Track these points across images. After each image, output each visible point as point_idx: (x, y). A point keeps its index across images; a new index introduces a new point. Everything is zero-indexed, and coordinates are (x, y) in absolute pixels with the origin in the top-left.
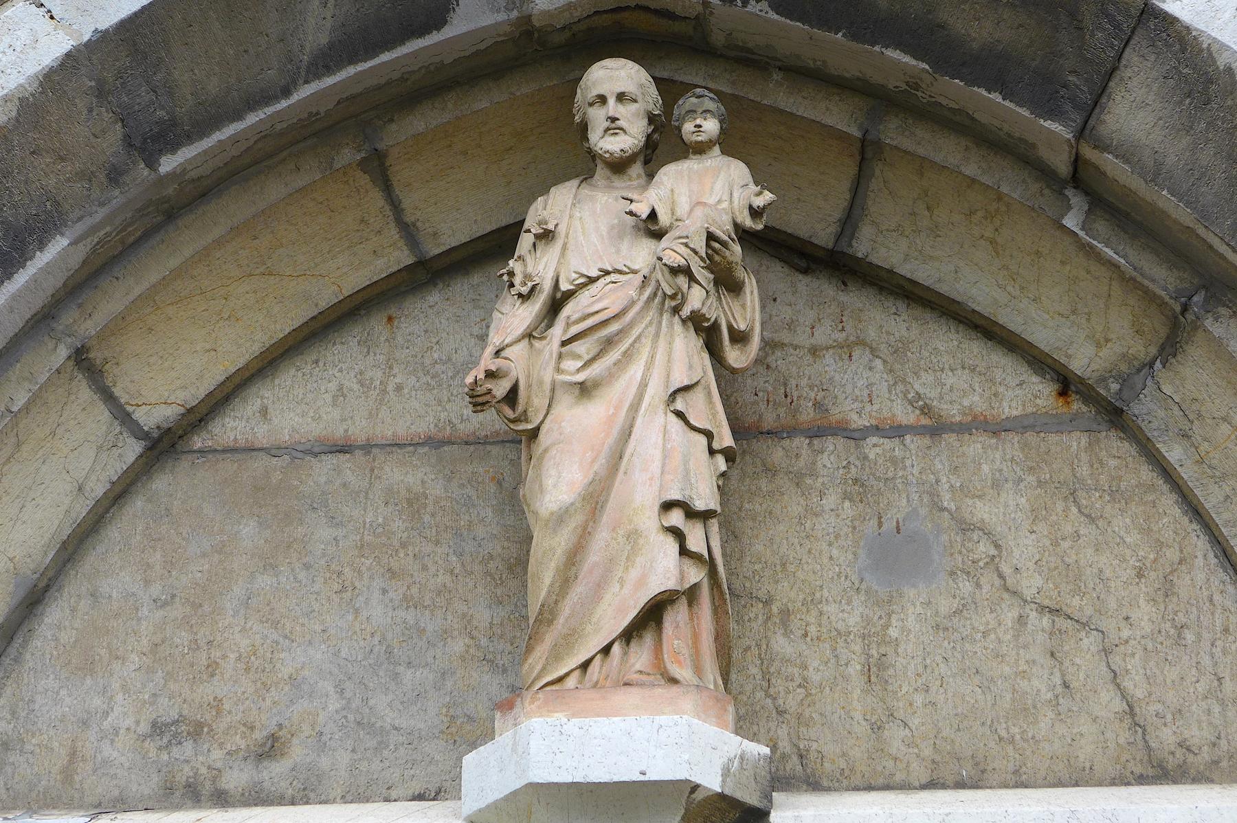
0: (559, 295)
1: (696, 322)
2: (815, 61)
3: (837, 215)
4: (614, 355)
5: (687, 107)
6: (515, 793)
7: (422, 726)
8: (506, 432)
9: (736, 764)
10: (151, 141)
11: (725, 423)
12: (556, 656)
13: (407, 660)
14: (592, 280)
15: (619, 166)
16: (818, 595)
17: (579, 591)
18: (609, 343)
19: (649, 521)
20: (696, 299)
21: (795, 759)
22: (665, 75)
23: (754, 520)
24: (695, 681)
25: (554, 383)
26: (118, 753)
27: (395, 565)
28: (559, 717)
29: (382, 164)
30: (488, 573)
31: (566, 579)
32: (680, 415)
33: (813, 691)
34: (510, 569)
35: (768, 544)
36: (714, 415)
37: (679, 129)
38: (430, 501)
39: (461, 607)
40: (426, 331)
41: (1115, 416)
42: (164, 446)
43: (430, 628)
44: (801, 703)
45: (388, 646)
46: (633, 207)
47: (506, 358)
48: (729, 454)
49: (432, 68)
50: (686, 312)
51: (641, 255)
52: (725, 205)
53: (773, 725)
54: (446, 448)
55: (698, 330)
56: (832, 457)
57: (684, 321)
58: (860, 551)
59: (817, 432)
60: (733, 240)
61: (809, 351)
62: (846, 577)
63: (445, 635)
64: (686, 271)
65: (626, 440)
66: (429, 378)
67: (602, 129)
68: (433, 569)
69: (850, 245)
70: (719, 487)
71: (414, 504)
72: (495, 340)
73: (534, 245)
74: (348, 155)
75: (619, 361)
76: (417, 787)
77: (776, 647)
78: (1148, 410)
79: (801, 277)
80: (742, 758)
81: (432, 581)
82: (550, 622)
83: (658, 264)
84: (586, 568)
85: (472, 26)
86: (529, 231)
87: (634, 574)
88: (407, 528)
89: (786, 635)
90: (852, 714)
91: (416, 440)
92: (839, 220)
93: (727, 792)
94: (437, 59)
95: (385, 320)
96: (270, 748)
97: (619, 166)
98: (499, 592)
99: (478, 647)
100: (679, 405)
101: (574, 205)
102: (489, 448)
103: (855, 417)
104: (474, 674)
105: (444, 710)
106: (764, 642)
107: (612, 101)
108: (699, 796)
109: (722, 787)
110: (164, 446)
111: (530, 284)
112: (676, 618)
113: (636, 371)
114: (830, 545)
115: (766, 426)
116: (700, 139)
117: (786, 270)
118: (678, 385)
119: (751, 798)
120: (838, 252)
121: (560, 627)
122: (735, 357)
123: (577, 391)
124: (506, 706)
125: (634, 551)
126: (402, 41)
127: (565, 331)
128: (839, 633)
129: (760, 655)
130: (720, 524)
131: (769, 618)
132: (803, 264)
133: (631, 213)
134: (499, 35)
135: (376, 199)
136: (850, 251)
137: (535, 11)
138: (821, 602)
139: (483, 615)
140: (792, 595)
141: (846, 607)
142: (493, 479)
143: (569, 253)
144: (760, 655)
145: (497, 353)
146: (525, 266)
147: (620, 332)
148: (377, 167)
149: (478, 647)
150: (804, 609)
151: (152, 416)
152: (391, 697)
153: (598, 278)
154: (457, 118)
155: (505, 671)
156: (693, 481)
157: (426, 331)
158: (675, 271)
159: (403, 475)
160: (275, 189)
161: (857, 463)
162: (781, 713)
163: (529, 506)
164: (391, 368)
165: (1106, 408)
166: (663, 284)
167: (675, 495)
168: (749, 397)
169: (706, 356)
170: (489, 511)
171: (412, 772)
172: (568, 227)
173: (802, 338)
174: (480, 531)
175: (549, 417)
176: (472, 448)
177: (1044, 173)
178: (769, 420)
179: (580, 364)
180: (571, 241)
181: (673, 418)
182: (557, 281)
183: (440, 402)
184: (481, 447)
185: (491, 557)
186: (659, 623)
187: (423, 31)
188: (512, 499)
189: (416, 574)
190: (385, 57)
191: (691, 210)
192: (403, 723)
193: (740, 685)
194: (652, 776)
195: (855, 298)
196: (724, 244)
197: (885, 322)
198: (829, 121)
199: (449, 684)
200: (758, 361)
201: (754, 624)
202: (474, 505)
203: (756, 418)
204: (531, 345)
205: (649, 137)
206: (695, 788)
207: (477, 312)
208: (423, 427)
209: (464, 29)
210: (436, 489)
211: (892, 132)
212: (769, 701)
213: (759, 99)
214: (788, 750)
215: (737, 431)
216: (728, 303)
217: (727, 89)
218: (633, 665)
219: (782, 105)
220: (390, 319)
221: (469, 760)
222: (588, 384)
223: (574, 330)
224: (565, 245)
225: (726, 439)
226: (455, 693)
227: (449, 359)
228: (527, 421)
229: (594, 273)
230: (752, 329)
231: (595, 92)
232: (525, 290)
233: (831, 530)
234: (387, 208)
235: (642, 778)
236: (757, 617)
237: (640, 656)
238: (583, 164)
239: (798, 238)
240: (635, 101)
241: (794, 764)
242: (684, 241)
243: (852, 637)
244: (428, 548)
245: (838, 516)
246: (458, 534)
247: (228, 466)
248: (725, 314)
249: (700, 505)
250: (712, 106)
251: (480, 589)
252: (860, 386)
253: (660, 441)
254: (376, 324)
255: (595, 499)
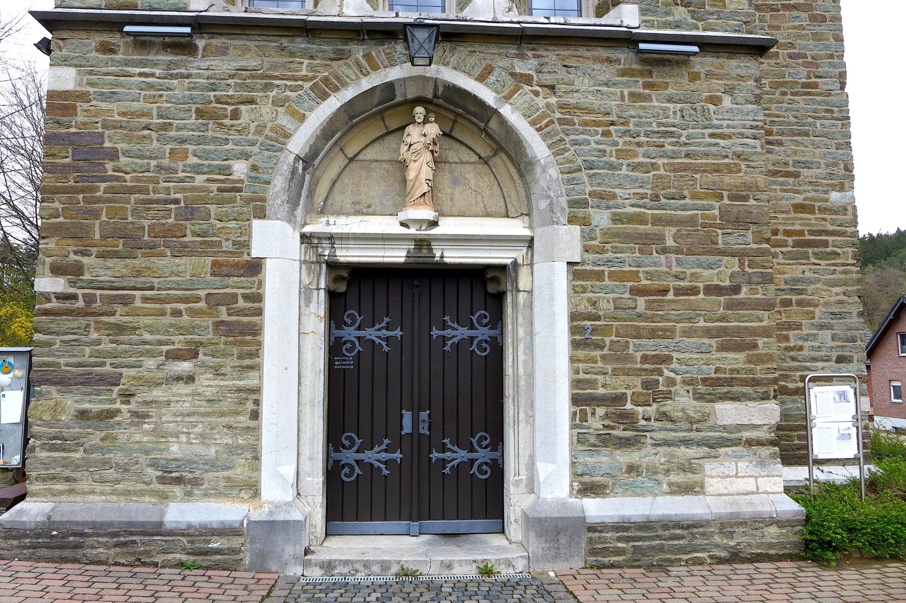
10: (351, 118)
19: (424, 181)
26: (348, 206)
41: (486, 163)
42: (351, 160)
51: (423, 139)
59: (445, 163)
65: (420, 169)
71: (388, 170)
74: (379, 118)
78: (490, 163)
96: (369, 206)
110: (351, 160)
130: (544, 461)
135: (382, 123)
139: (398, 188)
148: (383, 119)
151: (349, 156)
159: (385, 166)
160: (368, 123)
165: (485, 161)
177: (480, 128)
195: (451, 141)
197: (456, 145)
208: (389, 158)
211: (459, 120)
237: (422, 199)
247: (360, 163)
252: (452, 156)
254: (381, 141)
255: (416, 177)
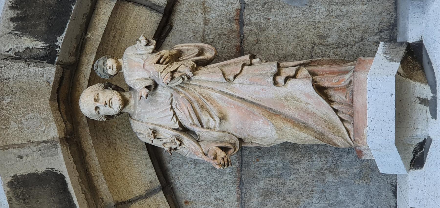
0: (181, 129)
1: (194, 70)
2: (83, 19)
3: (149, 12)
4: (208, 105)
5: (101, 72)
6: (399, 150)
7: (363, 192)
8: (237, 154)
9: (388, 56)
11: (239, 59)
12: (339, 132)
13: (335, 197)
14: (175, 114)
15: (125, 102)
16: (312, 23)
17: (310, 122)
18: (202, 107)
20: (184, 68)
21: (382, 34)
22: (87, 82)
23: (279, 49)
24: (351, 73)
25: (219, 131)
27: (294, 202)
28: (366, 131)
29: (121, 203)
30: (298, 162)
31: (306, 127)
32: (235, 77)
33: (353, 26)
34: (297, 153)
35: (289, 43)
36: (235, 63)
37: (111, 76)
38: (266, 187)
39: (313, 174)
40: (192, 187)
43: (321, 188)
44: (358, 31)
45: (329, 205)
46: (144, 96)
47: (208, 151)
48: (253, 57)
49: (80, 181)
50: (190, 74)
51: (163, 93)
52: (144, 57)
53: (367, 43)
54: (243, 180)
55: (197, 69)
56: (252, 16)
57: (194, 75)
58: (293, 5)
60: (160, 53)
61: (206, 25)
62: (304, 11)
63: (324, 181)
64: (173, 72)
66: (212, 187)
67: (110, 109)
68: (296, 186)
69: (162, 7)
70: (266, 62)
71: (267, 194)
72: (200, 157)
73: (158, 139)
75: (211, 103)
76: (390, 195)
77: (334, 41)
79: (174, 28)
80: (385, 54)
81: (301, 186)
82: (323, 135)
83: (169, 85)
84: (300, 119)
85: (63, 163)
86: (152, 141)
87: (304, 98)
88: (278, 197)
89: (328, 37)
90: (363, 10)
91: (239, 192)
92: (151, 11)
93: (400, 60)
94: (77, 178)
95: (187, 205)
97: (125, 102)
98: (306, 158)
99: (330, 167)
100: (231, 77)
101: (141, 121)
102: (244, 162)
103: (235, 6)
104: (342, 169)
105: (357, 182)
106: (331, 46)
107: (98, 104)
108: (402, 72)
109: (398, 62)
111: (176, 141)
112: (323, 82)
113: (215, 95)
114: (290, 17)
115: (238, 43)
116: (115, 67)
117: (171, 34)
118: (223, 78)
119: (402, 51)
120: (164, 12)
121: (325, 131)
122: (208, 55)
123: (224, 121)
124: (360, 153)
125: (294, 98)
126: (69, 193)
127: (197, 126)
128: (328, 14)
129: (337, 48)
131: (321, 44)
132: (168, 27)
133: (147, 96)
134: (67, 152)
136: (164, 7)
137: (58, 136)
138: (315, 22)
139: (317, 165)
140: (311, 34)
141: (317, 12)
142: (257, 160)
143: (163, 124)
144: (337, 48)
145: (206, 155)
146: (167, 143)
147: (198, 102)
149: (330, 167)
150: (318, 29)
152: (350, 205)
153: (174, 111)
154: (102, 171)
155: (341, 156)
156: (264, 72)
157: (192, 187)
158: (172, 78)
161: (255, 6)
162: (362, 40)
163: (272, 143)
164: (208, 202)
166: (178, 83)
167: (271, 79)
168: (226, 50)
169: (209, 66)
170: (271, 162)
171: (383, 196)
172: (151, 124)
173: (200, 28)
174: (280, 166)
175: (234, 133)
176: (244, 169)
178: (236, 42)
179: (211, 119)
180: (157, 123)
181: (236, 80)
182: (174, 129)
183: (223, 182)
184: (243, 165)
185: (291, 161)
186: (325, 88)
187: (65, 184)
188: (266, 152)
189: (297, 193)
190: (75, 200)
191: (147, 70)
192: (362, 200)
193: (354, 53)
194: (393, 91)
196: (161, 57)
198: (109, 13)
199: (346, 180)
200: (211, 43)
201: (324, 50)
202: (269, 168)
203: (235, 48)
204: (202, 141)
205: (113, 89)
206: (398, 73)
207: (184, 166)
208: (234, 189)
209: (65, 166)
210: (261, 184)
212: (356, 45)
213: (99, 43)
214: (378, 37)
215: (241, 53)
216: (187, 56)
217: (94, 56)
218: (343, 100)
219: (102, 33)
220: (186, 202)
221: (382, 170)
222: (220, 116)
223: (196, 122)
224: (158, 125)
225: (246, 58)
226: (350, 177)
227: (205, 178)
228: (235, 143)
229: (172, 113)
230: (198, 47)
231: (94, 111)
232: (178, 143)
233: (284, 17)
234: (139, 202)
235: (394, 95)
236: (321, 49)
238: (123, 118)
239: (158, 29)
240: (98, 94)
241: (385, 35)
242: (160, 73)
243: (330, 9)
244: (287, 188)
245: (278, 14)
246: (281, 175)
248: (191, 57)
249: (275, 69)
250: (101, 62)
251: (305, 166)
253: (246, 86)
255: (272, 113)
